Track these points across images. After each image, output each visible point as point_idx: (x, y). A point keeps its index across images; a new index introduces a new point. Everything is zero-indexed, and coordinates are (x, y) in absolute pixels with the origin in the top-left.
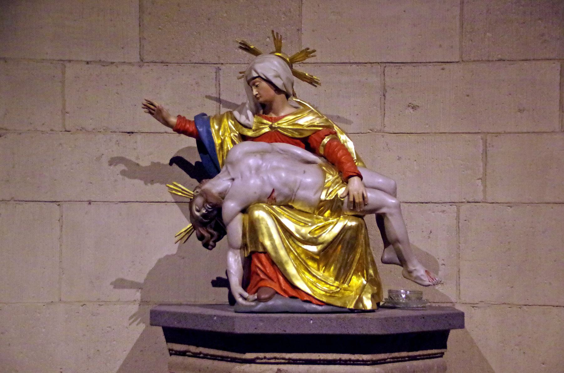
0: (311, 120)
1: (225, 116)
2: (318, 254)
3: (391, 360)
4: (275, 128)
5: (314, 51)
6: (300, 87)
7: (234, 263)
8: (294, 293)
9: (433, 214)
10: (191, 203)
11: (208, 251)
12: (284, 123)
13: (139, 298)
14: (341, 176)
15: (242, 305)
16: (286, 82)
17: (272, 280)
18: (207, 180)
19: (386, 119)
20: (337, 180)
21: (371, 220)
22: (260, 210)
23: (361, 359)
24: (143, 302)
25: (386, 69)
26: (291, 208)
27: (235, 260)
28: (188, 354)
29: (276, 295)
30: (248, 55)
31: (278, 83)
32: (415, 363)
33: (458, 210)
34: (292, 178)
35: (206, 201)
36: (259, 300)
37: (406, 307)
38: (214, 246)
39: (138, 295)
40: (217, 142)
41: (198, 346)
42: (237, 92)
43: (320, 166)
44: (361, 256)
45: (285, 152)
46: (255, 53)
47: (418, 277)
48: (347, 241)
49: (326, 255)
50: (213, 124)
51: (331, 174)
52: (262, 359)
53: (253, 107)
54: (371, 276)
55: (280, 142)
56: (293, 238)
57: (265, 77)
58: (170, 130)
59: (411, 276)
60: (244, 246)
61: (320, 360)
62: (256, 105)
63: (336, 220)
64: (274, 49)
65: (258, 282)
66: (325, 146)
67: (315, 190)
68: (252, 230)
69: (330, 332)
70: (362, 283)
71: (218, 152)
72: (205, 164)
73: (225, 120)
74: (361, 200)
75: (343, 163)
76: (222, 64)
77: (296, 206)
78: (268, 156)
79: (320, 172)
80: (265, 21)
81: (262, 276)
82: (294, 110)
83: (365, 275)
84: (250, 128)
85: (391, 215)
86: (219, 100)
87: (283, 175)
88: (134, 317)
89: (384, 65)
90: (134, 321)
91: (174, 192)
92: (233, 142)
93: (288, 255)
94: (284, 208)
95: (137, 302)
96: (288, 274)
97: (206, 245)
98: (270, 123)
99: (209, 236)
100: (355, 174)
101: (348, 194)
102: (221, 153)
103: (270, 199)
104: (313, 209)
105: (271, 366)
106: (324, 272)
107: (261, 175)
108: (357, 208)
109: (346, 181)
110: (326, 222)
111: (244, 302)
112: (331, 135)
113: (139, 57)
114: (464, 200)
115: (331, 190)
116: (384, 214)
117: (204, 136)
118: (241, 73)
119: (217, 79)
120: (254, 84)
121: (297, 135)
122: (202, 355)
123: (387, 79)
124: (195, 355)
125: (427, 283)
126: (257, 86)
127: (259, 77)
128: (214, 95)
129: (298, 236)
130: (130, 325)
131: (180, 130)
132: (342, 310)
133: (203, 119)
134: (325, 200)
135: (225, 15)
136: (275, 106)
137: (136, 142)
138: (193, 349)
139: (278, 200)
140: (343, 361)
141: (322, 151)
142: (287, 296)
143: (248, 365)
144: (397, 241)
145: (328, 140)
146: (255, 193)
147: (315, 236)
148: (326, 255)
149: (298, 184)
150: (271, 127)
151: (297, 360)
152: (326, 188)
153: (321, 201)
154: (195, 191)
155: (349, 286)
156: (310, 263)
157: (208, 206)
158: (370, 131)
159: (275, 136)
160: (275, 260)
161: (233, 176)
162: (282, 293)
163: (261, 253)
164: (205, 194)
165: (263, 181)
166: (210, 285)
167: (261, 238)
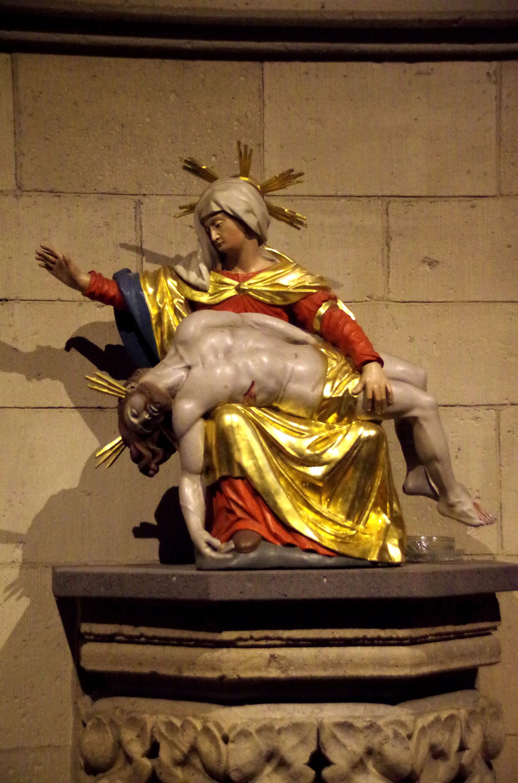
0: (299, 279)
1: (162, 274)
2: (321, 479)
3: (434, 638)
4: (244, 290)
5: (301, 174)
6: (276, 230)
7: (192, 496)
8: (289, 539)
9: (462, 422)
10: (122, 403)
11: (147, 478)
12: (259, 281)
13: (20, 560)
14: (349, 361)
15: (212, 558)
16: (261, 221)
17: (257, 520)
18: (145, 369)
19: (391, 280)
20: (345, 368)
21: (389, 426)
22: (233, 413)
23: (394, 636)
24: (27, 564)
25: (391, 205)
26: (277, 410)
27: (194, 491)
28: (117, 638)
29: (263, 542)
30: (195, 180)
31: (251, 221)
32: (463, 642)
33: (499, 417)
34: (279, 364)
35: (151, 401)
36: (238, 550)
37: (433, 559)
38: (156, 471)
39: (17, 553)
40: (153, 312)
41: (136, 625)
42: (183, 238)
43: (316, 348)
44: (382, 482)
45: (263, 326)
46: (209, 177)
47: (464, 514)
48: (363, 460)
49: (331, 483)
50: (145, 285)
51: (334, 359)
52: (246, 640)
53: (208, 258)
54: (396, 512)
55: (251, 312)
56: (282, 455)
57: (232, 211)
58: (78, 295)
59: (453, 512)
60: (207, 470)
61: (334, 639)
62: (211, 255)
63: (345, 427)
64: (238, 172)
65: (233, 523)
66: (322, 318)
67: (313, 383)
68: (223, 445)
69: (352, 596)
70: (384, 522)
71: (154, 328)
72: (131, 346)
73: (162, 279)
74: (384, 397)
75: (353, 342)
76: (144, 195)
77: (285, 408)
78: (240, 332)
79: (318, 357)
80: (209, 131)
81: (239, 513)
82: (269, 264)
83: (388, 510)
84: (205, 291)
85: (426, 419)
86: (140, 250)
87: (265, 359)
88: (12, 588)
89: (387, 199)
90: (12, 594)
91: (96, 387)
92: (177, 312)
93: (279, 482)
94: (266, 410)
95: (18, 564)
96: (280, 510)
97: (146, 470)
98: (236, 283)
99: (151, 455)
100: (374, 359)
101: (364, 388)
102: (159, 329)
103: (247, 397)
104: (310, 411)
105: (259, 651)
106: (328, 506)
107: (234, 361)
108: (375, 408)
109: (359, 369)
110: (332, 432)
111: (213, 554)
112: (330, 301)
113: (14, 182)
114: (506, 402)
115: (337, 382)
116: (415, 419)
117: (133, 302)
118: (181, 208)
119: (137, 217)
120: (213, 224)
121: (278, 301)
122: (143, 639)
123: (392, 220)
124: (131, 640)
125: (477, 521)
126: (218, 226)
127: (223, 211)
128: (133, 243)
129: (293, 453)
130: (5, 601)
131: (95, 295)
132: (360, 563)
133: (123, 277)
134: (331, 398)
135: (148, 120)
136: (244, 256)
137: (12, 315)
138: (128, 630)
139: (259, 398)
140: (368, 639)
141: (317, 325)
142: (279, 544)
143: (225, 650)
144: (435, 458)
145: (327, 307)
146: (226, 387)
147: (317, 452)
148: (331, 483)
149: (288, 375)
150: (238, 289)
151: (299, 640)
152: (329, 380)
153: (324, 399)
154: (129, 386)
155: (366, 528)
156: (308, 494)
157: (153, 408)
158: (368, 299)
159: (244, 302)
160: (259, 489)
161: (188, 362)
162: (271, 539)
163: (237, 478)
164: (146, 390)
165: (237, 370)
166: (132, 535)
167: (236, 456)
